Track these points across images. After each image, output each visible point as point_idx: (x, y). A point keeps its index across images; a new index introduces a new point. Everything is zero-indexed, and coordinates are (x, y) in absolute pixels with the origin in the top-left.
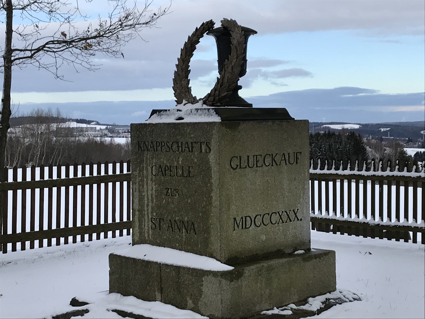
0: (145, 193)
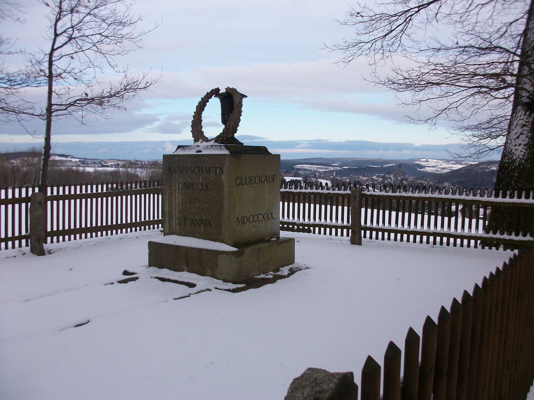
0: (174, 201)
